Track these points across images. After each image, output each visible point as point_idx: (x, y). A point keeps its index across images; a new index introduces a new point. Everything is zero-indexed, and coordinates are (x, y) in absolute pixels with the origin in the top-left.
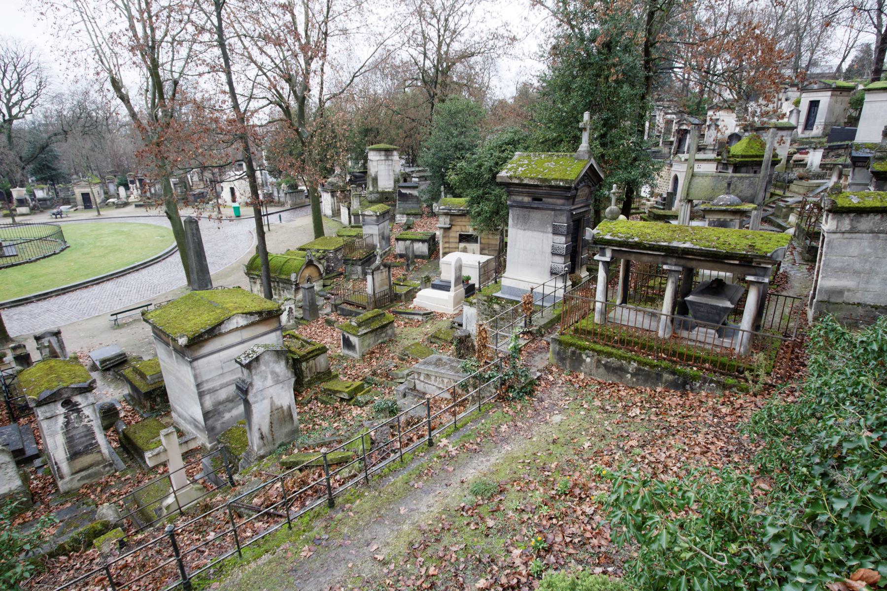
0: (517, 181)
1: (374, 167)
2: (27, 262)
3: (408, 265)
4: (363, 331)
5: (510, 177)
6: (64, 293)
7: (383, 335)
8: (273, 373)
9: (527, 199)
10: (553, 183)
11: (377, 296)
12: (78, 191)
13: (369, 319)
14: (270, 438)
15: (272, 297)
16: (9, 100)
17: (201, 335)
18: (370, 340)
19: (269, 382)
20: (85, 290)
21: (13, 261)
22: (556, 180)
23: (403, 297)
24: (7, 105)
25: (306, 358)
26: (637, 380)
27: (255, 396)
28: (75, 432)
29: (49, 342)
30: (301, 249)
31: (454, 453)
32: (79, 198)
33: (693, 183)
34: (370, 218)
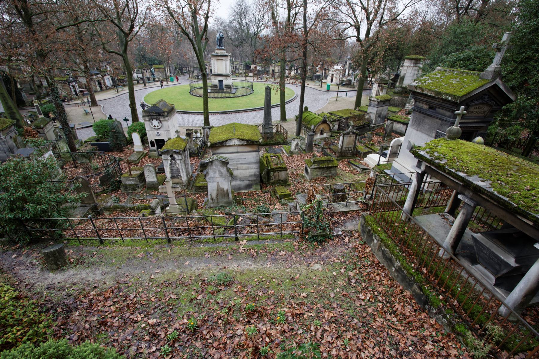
1: (404, 70)
3: (385, 137)
4: (314, 166)
5: (416, 87)
7: (328, 172)
8: (219, 171)
9: (425, 107)
10: (444, 97)
11: (344, 149)
12: (271, 68)
13: (322, 161)
14: (216, 201)
16: (259, 24)
17: (217, 144)
18: (318, 172)
19: (217, 175)
21: (234, 95)
22: (447, 94)
23: (362, 155)
25: (274, 170)
27: (209, 179)
28: (173, 168)
30: (330, 113)
31: (240, 251)
32: (271, 72)
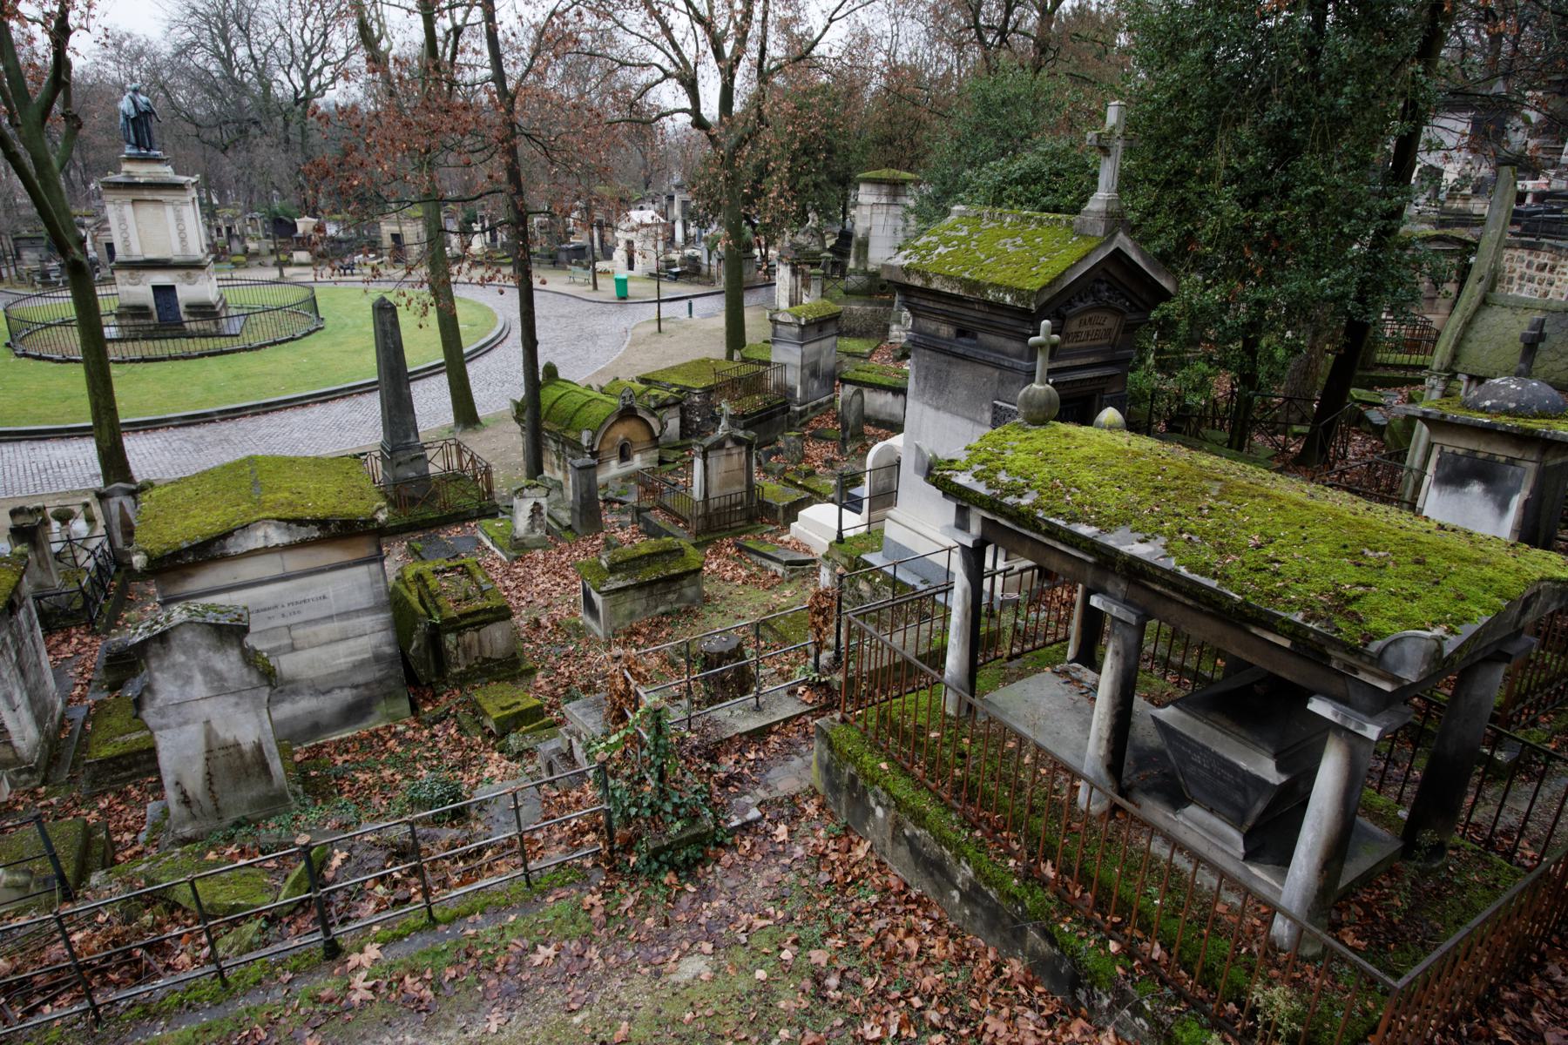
0: (918, 282)
1: (864, 217)
2: (245, 349)
4: (615, 582)
5: (907, 271)
6: (266, 413)
8: (207, 670)
9: (946, 331)
10: (991, 295)
11: (714, 504)
12: (387, 229)
13: (641, 557)
14: (208, 805)
15: (541, 472)
16: (308, 64)
17: (179, 553)
19: (199, 688)
20: (299, 411)
22: (997, 287)
23: (781, 514)
24: (304, 72)
25: (455, 625)
26: (973, 914)
27: (161, 712)
29: (121, 504)
30: (643, 380)
32: (387, 242)
33: (1478, 325)
34: (786, 328)
